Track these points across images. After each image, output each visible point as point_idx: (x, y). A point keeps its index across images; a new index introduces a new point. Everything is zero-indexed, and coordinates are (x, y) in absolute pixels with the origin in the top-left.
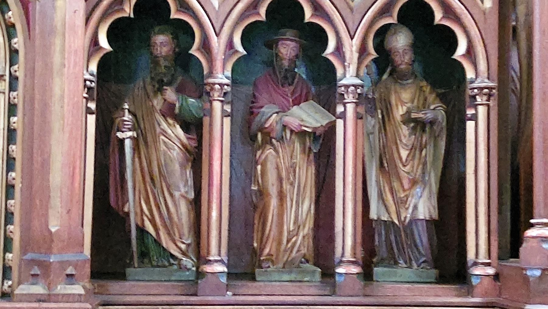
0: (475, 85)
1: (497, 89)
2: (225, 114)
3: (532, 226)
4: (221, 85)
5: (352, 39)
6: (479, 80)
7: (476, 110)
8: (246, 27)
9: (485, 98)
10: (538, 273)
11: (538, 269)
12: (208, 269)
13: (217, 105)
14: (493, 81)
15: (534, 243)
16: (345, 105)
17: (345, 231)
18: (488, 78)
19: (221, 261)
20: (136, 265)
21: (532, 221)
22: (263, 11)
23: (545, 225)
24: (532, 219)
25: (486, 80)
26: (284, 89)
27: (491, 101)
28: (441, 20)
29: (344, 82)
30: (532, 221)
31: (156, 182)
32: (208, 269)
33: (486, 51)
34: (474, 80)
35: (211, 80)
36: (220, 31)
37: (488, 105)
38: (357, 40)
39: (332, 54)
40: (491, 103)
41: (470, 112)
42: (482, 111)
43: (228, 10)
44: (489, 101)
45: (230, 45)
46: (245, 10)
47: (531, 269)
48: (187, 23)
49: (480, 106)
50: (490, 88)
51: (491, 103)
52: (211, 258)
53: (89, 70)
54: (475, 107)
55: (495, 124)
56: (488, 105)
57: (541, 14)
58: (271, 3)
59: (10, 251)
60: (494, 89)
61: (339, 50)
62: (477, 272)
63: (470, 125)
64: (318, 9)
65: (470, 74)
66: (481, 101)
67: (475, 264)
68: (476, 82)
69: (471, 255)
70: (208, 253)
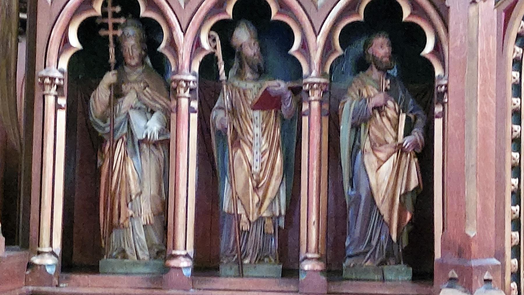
2: (191, 110)
4: (187, 82)
5: (316, 36)
8: (156, 21)
12: (173, 263)
13: (184, 102)
16: (310, 102)
17: (176, 220)
19: (187, 256)
20: (480, 287)
22: (230, 10)
26: (243, 85)
28: (409, 16)
29: (310, 80)
32: (173, 263)
35: (177, 77)
36: (186, 29)
38: (322, 36)
39: (298, 51)
43: (173, 7)
44: (385, 91)
45: (197, 44)
46: (297, 16)
48: (159, 25)
52: (178, 252)
53: (59, 68)
55: (108, 91)
58: (236, 3)
61: (304, 46)
64: (284, 7)
70: (174, 248)
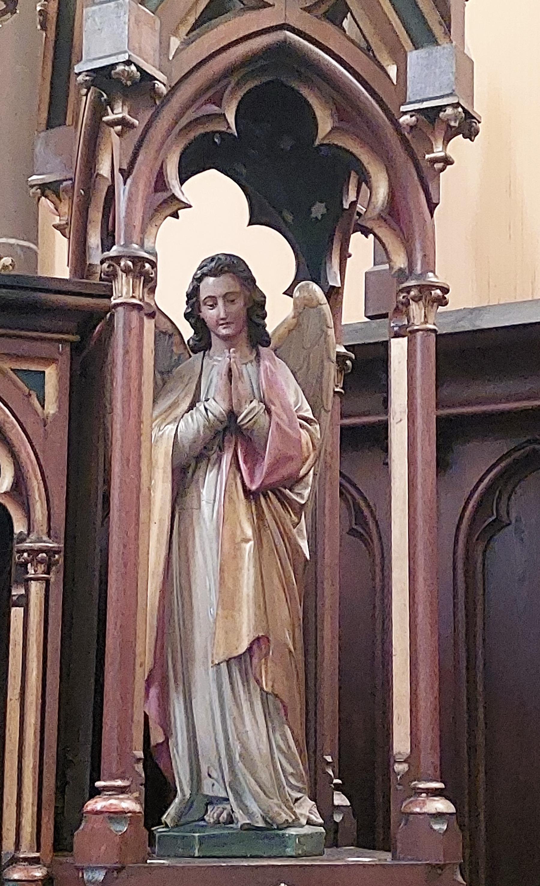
0: (26, 545)
1: (62, 554)
3: (95, 792)
6: (33, 537)
7: (27, 590)
9: (41, 568)
10: (100, 876)
11: (102, 868)
14: (56, 539)
15: (97, 823)
18: (49, 536)
21: (98, 784)
23: (116, 791)
24: (99, 780)
25: (45, 538)
27: (51, 574)
30: (98, 784)
31: (373, 538)
33: (46, 490)
34: (25, 537)
37: (47, 581)
40: (52, 577)
41: (17, 591)
42: (36, 588)
44: (49, 574)
47: (93, 869)
49: (32, 582)
50: (49, 551)
51: (52, 577)
54: (26, 583)
56: (47, 581)
57: (352, 340)
59: (473, 138)
60: (58, 552)
62: (16, 876)
63: (17, 613)
65: (19, 527)
66: (33, 572)
67: (14, 861)
68: (28, 540)
69: (8, 844)
